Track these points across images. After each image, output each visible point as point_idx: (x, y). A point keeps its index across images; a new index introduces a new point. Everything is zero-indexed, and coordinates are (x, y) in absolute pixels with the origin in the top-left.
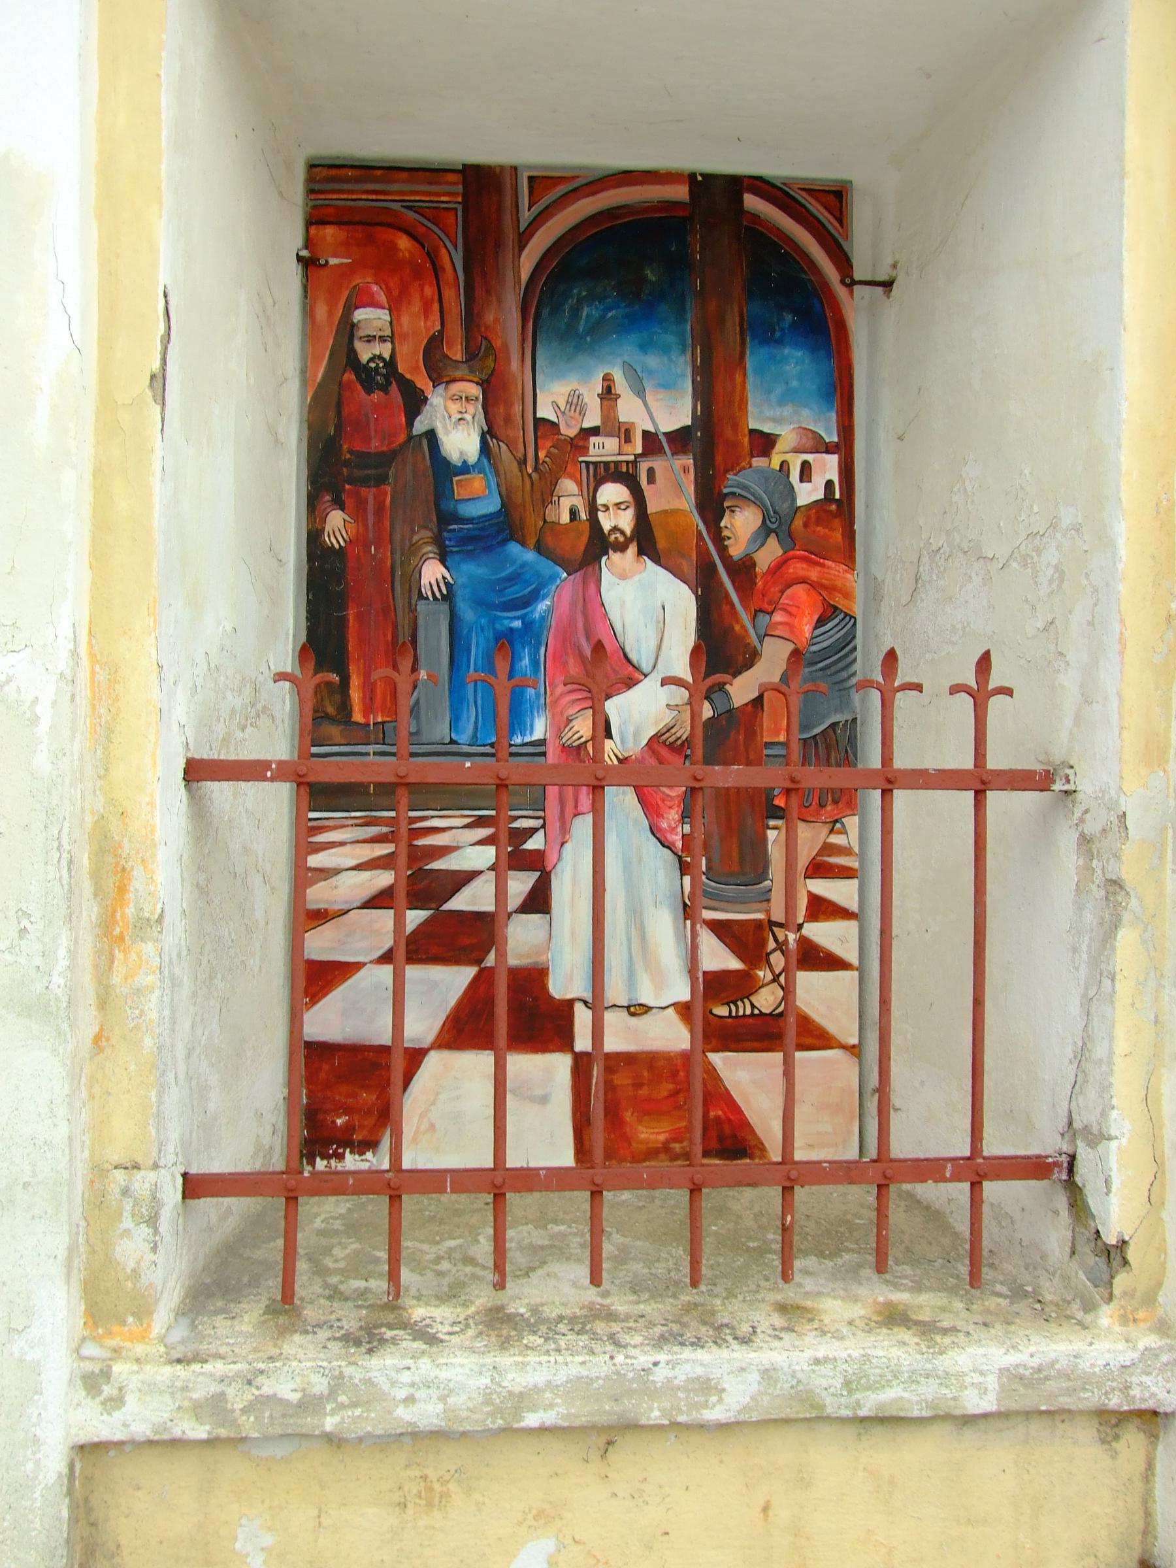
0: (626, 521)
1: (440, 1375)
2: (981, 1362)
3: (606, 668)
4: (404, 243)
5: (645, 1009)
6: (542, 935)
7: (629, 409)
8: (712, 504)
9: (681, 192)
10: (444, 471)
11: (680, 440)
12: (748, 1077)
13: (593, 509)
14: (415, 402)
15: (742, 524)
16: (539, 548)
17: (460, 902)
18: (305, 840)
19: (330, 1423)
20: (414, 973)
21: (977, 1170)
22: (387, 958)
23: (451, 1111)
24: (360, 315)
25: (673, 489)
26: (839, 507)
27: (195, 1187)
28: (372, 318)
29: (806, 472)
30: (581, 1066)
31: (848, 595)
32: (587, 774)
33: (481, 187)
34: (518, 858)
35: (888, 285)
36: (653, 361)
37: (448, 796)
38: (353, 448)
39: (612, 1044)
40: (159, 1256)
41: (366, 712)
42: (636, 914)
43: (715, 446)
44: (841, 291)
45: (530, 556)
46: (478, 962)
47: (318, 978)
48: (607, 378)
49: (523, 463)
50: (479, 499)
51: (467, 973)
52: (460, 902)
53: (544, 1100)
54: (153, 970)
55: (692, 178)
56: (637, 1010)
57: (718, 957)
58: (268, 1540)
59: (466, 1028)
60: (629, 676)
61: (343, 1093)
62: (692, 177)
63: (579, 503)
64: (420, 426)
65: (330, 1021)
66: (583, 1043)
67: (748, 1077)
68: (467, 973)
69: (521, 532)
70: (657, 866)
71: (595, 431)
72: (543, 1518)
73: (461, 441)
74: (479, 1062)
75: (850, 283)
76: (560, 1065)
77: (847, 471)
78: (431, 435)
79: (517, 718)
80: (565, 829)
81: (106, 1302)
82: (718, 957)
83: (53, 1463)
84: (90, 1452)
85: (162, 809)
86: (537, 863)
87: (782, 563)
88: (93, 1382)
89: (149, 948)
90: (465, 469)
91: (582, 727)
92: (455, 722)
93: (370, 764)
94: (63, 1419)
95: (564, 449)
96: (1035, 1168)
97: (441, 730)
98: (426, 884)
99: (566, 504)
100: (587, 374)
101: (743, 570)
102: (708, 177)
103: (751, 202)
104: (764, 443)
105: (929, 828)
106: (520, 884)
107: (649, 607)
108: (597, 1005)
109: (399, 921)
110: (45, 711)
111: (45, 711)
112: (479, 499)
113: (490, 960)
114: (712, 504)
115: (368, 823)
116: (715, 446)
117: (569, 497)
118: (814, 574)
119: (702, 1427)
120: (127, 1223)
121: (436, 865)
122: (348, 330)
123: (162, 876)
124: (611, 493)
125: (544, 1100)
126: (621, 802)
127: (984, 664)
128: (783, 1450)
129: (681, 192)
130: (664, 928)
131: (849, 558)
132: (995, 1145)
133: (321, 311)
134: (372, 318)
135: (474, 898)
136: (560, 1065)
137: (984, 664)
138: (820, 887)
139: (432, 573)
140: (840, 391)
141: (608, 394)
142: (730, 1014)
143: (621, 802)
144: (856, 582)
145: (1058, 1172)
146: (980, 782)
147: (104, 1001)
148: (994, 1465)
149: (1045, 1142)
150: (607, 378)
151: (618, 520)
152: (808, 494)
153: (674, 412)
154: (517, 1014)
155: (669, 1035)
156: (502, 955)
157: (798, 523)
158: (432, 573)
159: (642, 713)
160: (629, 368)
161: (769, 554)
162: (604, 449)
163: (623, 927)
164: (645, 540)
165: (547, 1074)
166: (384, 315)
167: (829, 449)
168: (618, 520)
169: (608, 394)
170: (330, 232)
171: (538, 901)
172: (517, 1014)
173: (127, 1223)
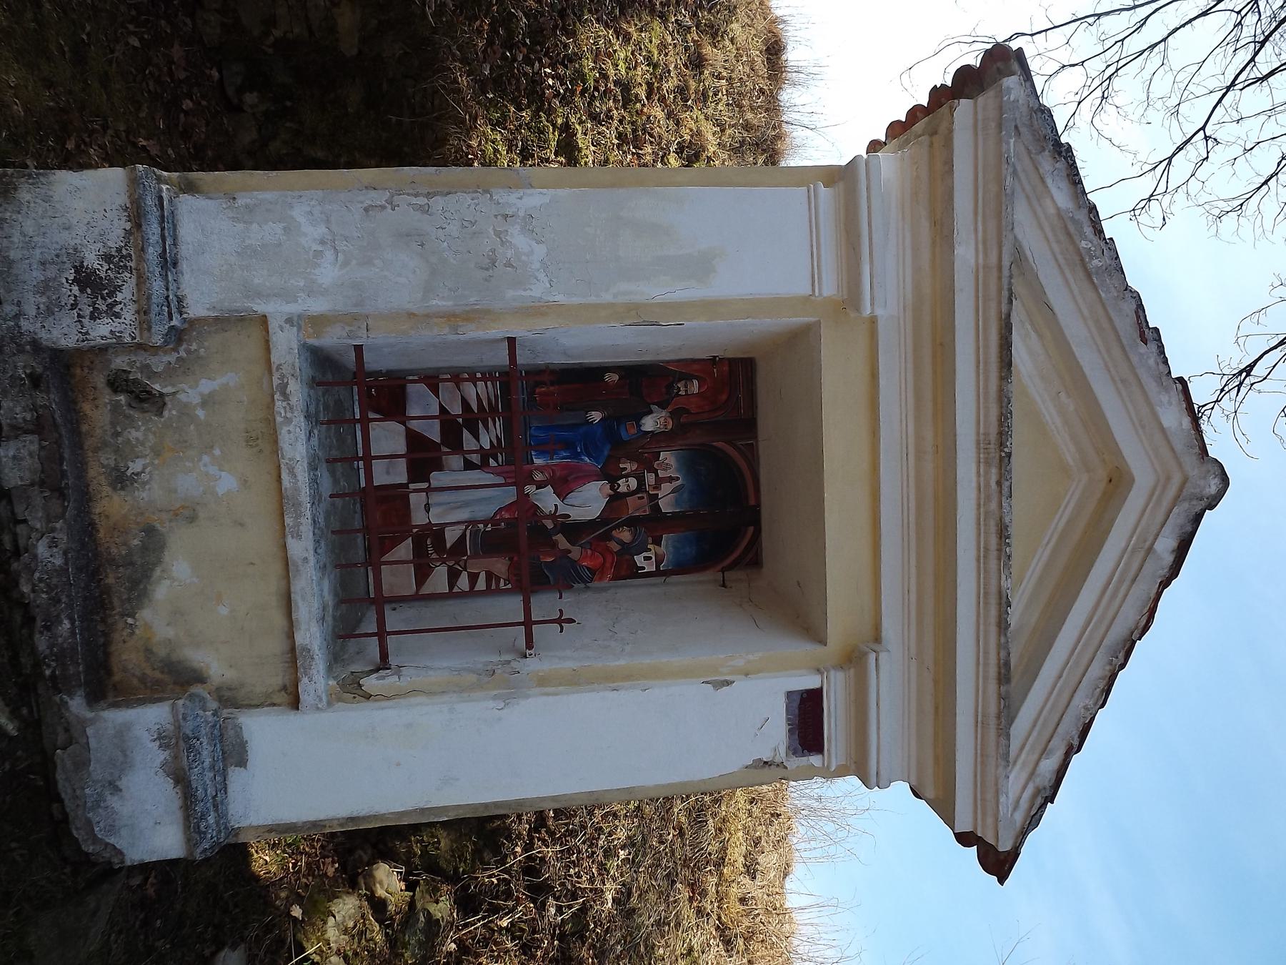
0: (623, 489)
1: (297, 443)
2: (311, 635)
3: (563, 487)
4: (724, 397)
5: (428, 511)
6: (455, 468)
7: (666, 488)
8: (632, 523)
9: (752, 502)
10: (638, 418)
11: (656, 508)
12: (404, 550)
13: (627, 476)
14: (663, 406)
15: (625, 535)
16: (609, 457)
17: (466, 434)
18: (488, 376)
19: (278, 404)
20: (437, 422)
21: (382, 634)
22: (443, 410)
23: (388, 438)
24: (695, 382)
25: (636, 507)
26: (634, 573)
27: (359, 349)
28: (695, 387)
29: (647, 558)
30: (406, 486)
31: (600, 579)
32: (519, 477)
33: (748, 425)
34: (485, 455)
35: (724, 585)
36: (685, 496)
37: (508, 428)
38: (645, 381)
39: (413, 497)
40: (332, 339)
41: (540, 394)
42: (466, 504)
43: (654, 523)
44: (720, 567)
45: (606, 453)
46: (444, 442)
47: (432, 380)
48: (678, 479)
49: (642, 448)
50: (628, 432)
51: (438, 440)
52: (466, 434)
53: (388, 473)
54: (442, 332)
55: (758, 505)
56: (427, 508)
57: (451, 536)
58: (231, 384)
59: (415, 440)
60: (562, 494)
61: (387, 394)
62: (759, 505)
63: (629, 470)
64: (654, 407)
65: (417, 390)
66: (412, 486)
67: (404, 550)
68: (438, 440)
69: (613, 450)
70: (487, 511)
71: (657, 475)
72: (245, 483)
73: (649, 424)
74: (401, 447)
75: (723, 571)
76: (403, 479)
77: (649, 575)
78: (651, 412)
79: (541, 453)
80: (498, 474)
81: (318, 322)
82: (451, 536)
83: (260, 307)
84: (264, 320)
85: (498, 331)
86: (483, 465)
87: (611, 552)
88: (289, 321)
89: (447, 330)
90: (639, 426)
91: (538, 477)
92: (538, 428)
93: (520, 397)
94: (275, 309)
95: (648, 463)
96: (384, 655)
97: (535, 424)
98: (472, 420)
99: (628, 466)
100: (678, 470)
101: (607, 536)
102: (759, 512)
103: (751, 529)
104: (657, 542)
105: (511, 607)
106: (475, 458)
107: (589, 501)
108: (428, 491)
109: (458, 416)
110: (528, 293)
111: (528, 293)
112: (628, 432)
113: (445, 449)
114: (632, 523)
115: (496, 396)
116: (654, 523)
117: (629, 466)
118: (608, 565)
119: (284, 536)
120: (348, 328)
121: (481, 425)
122: (688, 378)
123: (472, 332)
124: (633, 483)
125: (388, 473)
126: (509, 495)
127: (571, 621)
128: (277, 567)
129: (752, 502)
130: (464, 515)
131: (614, 579)
132: (391, 640)
133: (696, 367)
134: (695, 387)
135: (468, 441)
136: (403, 479)
137: (571, 621)
138: (483, 576)
139: (596, 416)
140: (680, 568)
141: (671, 479)
142: (430, 544)
143: (509, 495)
144: (605, 583)
145: (383, 664)
146: (528, 623)
147: (427, 316)
148: (274, 645)
149: (393, 660)
150: (678, 479)
151: (624, 485)
152: (639, 560)
153: (666, 505)
154: (422, 459)
155: (419, 518)
156: (448, 454)
157: (627, 557)
158: (596, 416)
159: (547, 500)
160: (682, 486)
161: (615, 547)
162: (650, 478)
163: (461, 500)
164: (616, 499)
165: (399, 474)
166: (696, 391)
167: (658, 567)
168: (624, 485)
169: (671, 479)
170: (726, 368)
171: (469, 466)
172: (422, 459)
173: (348, 328)
